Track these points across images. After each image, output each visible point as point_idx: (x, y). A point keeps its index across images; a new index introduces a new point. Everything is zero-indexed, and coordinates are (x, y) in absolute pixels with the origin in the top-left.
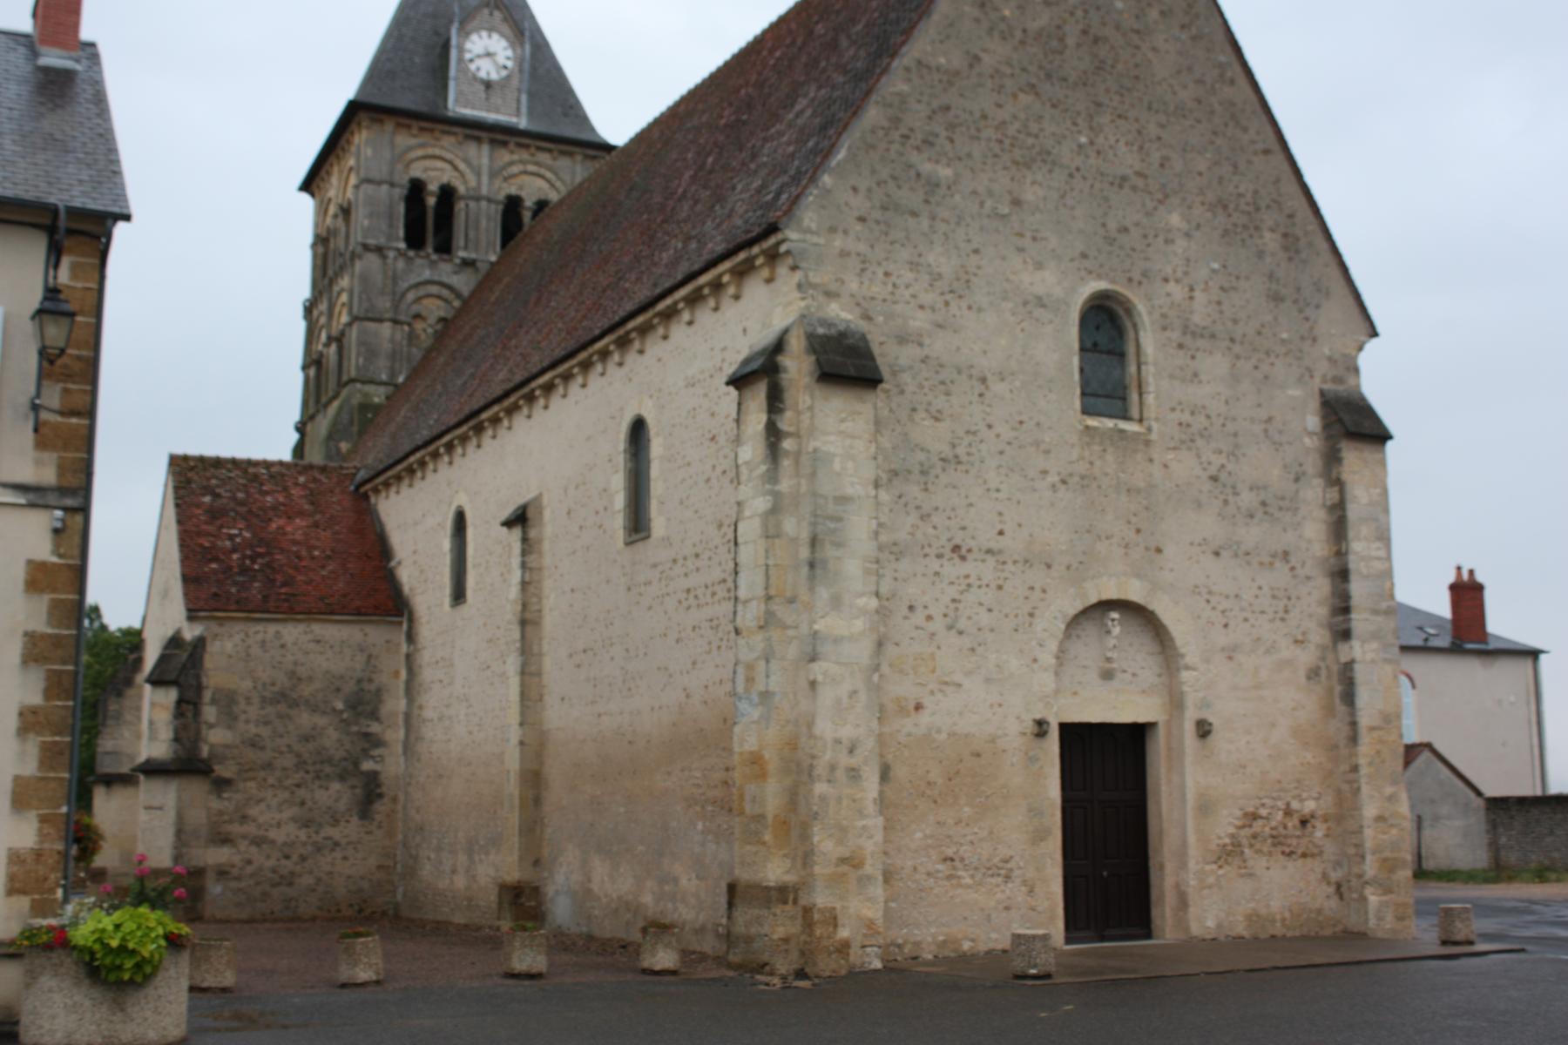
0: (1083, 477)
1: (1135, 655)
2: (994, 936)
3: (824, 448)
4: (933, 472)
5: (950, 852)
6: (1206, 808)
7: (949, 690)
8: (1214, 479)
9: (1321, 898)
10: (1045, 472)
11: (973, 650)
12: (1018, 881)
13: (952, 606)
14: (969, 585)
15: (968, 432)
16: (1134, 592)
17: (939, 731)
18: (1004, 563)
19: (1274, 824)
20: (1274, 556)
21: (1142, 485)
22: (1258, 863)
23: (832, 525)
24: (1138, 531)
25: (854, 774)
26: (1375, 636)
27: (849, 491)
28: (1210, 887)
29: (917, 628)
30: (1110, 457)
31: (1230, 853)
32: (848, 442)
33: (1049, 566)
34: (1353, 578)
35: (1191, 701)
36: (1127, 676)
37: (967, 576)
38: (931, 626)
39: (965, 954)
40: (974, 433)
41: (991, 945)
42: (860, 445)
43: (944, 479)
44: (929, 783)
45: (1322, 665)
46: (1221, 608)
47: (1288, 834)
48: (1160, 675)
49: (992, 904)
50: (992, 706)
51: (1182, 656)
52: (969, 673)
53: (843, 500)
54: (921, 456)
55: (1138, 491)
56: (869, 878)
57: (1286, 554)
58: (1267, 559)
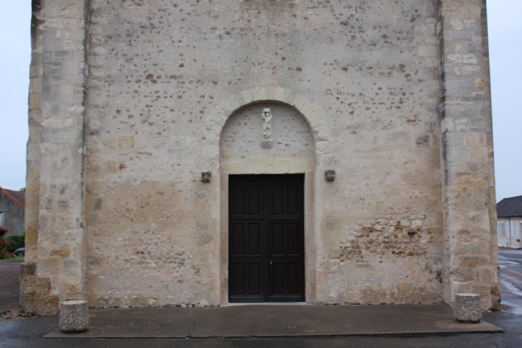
0: (242, 30)
1: (286, 132)
2: (170, 297)
3: (51, 26)
4: (135, 35)
5: (141, 249)
6: (331, 224)
7: (142, 157)
8: (345, 24)
9: (425, 281)
10: (215, 29)
11: (160, 133)
12: (188, 266)
13: (147, 109)
14: (158, 97)
15: (160, 10)
17: (135, 180)
18: (183, 83)
19: (386, 235)
20: (392, 68)
21: (287, 31)
22: (374, 260)
23: (54, 68)
24: (283, 59)
25: (64, 205)
26: (464, 114)
27: (66, 48)
28: (333, 273)
29: (122, 123)
30: (263, 16)
31: (352, 252)
32: (66, 21)
33: (215, 83)
34: (447, 77)
35: (322, 158)
36: (283, 146)
37: (157, 92)
38: (132, 121)
39: (150, 307)
40: (165, 10)
41: (168, 302)
42: (74, 22)
43: (142, 38)
44: (128, 209)
45: (430, 135)
46: (347, 102)
47: (403, 241)
49: (170, 279)
50: (173, 165)
51: (317, 132)
52: (157, 147)
53: (64, 53)
54: (128, 26)
55: (284, 35)
56: (72, 262)
57: (402, 67)
58: (386, 71)
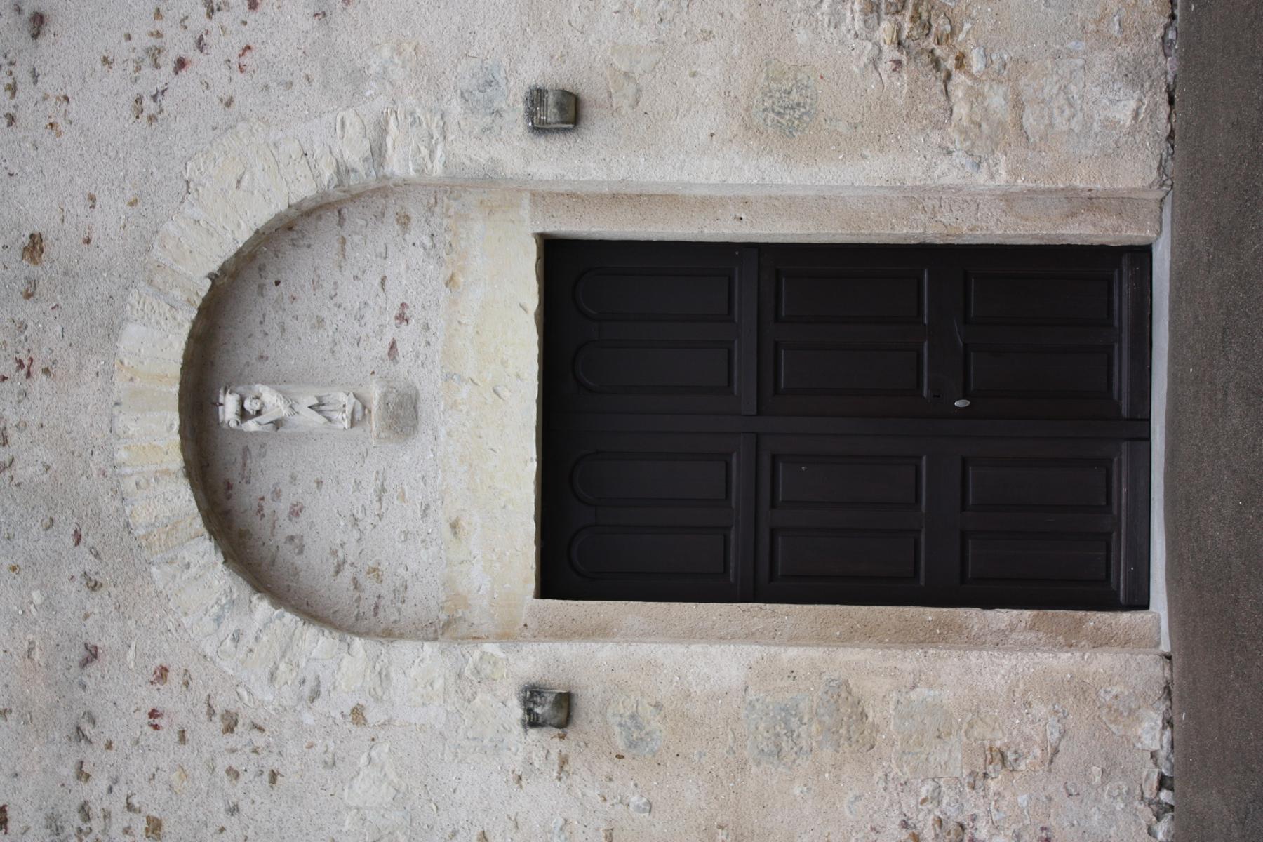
12: (973, 803)
16: (156, 346)
28: (1018, 105)
48: (404, 221)
